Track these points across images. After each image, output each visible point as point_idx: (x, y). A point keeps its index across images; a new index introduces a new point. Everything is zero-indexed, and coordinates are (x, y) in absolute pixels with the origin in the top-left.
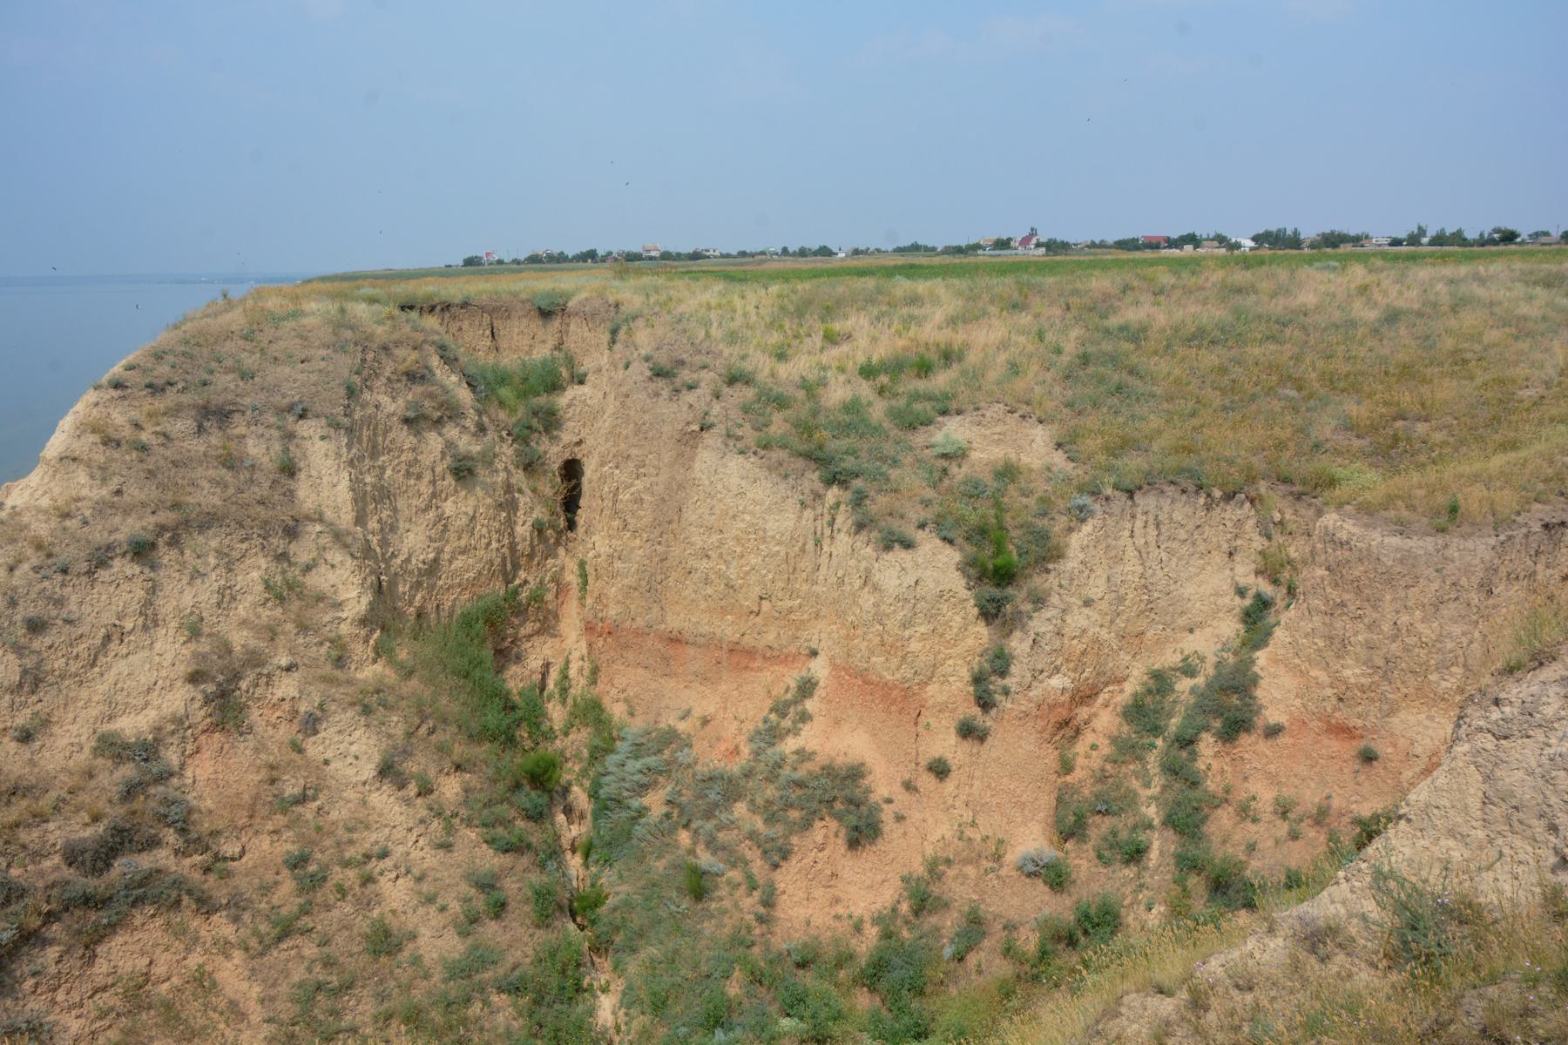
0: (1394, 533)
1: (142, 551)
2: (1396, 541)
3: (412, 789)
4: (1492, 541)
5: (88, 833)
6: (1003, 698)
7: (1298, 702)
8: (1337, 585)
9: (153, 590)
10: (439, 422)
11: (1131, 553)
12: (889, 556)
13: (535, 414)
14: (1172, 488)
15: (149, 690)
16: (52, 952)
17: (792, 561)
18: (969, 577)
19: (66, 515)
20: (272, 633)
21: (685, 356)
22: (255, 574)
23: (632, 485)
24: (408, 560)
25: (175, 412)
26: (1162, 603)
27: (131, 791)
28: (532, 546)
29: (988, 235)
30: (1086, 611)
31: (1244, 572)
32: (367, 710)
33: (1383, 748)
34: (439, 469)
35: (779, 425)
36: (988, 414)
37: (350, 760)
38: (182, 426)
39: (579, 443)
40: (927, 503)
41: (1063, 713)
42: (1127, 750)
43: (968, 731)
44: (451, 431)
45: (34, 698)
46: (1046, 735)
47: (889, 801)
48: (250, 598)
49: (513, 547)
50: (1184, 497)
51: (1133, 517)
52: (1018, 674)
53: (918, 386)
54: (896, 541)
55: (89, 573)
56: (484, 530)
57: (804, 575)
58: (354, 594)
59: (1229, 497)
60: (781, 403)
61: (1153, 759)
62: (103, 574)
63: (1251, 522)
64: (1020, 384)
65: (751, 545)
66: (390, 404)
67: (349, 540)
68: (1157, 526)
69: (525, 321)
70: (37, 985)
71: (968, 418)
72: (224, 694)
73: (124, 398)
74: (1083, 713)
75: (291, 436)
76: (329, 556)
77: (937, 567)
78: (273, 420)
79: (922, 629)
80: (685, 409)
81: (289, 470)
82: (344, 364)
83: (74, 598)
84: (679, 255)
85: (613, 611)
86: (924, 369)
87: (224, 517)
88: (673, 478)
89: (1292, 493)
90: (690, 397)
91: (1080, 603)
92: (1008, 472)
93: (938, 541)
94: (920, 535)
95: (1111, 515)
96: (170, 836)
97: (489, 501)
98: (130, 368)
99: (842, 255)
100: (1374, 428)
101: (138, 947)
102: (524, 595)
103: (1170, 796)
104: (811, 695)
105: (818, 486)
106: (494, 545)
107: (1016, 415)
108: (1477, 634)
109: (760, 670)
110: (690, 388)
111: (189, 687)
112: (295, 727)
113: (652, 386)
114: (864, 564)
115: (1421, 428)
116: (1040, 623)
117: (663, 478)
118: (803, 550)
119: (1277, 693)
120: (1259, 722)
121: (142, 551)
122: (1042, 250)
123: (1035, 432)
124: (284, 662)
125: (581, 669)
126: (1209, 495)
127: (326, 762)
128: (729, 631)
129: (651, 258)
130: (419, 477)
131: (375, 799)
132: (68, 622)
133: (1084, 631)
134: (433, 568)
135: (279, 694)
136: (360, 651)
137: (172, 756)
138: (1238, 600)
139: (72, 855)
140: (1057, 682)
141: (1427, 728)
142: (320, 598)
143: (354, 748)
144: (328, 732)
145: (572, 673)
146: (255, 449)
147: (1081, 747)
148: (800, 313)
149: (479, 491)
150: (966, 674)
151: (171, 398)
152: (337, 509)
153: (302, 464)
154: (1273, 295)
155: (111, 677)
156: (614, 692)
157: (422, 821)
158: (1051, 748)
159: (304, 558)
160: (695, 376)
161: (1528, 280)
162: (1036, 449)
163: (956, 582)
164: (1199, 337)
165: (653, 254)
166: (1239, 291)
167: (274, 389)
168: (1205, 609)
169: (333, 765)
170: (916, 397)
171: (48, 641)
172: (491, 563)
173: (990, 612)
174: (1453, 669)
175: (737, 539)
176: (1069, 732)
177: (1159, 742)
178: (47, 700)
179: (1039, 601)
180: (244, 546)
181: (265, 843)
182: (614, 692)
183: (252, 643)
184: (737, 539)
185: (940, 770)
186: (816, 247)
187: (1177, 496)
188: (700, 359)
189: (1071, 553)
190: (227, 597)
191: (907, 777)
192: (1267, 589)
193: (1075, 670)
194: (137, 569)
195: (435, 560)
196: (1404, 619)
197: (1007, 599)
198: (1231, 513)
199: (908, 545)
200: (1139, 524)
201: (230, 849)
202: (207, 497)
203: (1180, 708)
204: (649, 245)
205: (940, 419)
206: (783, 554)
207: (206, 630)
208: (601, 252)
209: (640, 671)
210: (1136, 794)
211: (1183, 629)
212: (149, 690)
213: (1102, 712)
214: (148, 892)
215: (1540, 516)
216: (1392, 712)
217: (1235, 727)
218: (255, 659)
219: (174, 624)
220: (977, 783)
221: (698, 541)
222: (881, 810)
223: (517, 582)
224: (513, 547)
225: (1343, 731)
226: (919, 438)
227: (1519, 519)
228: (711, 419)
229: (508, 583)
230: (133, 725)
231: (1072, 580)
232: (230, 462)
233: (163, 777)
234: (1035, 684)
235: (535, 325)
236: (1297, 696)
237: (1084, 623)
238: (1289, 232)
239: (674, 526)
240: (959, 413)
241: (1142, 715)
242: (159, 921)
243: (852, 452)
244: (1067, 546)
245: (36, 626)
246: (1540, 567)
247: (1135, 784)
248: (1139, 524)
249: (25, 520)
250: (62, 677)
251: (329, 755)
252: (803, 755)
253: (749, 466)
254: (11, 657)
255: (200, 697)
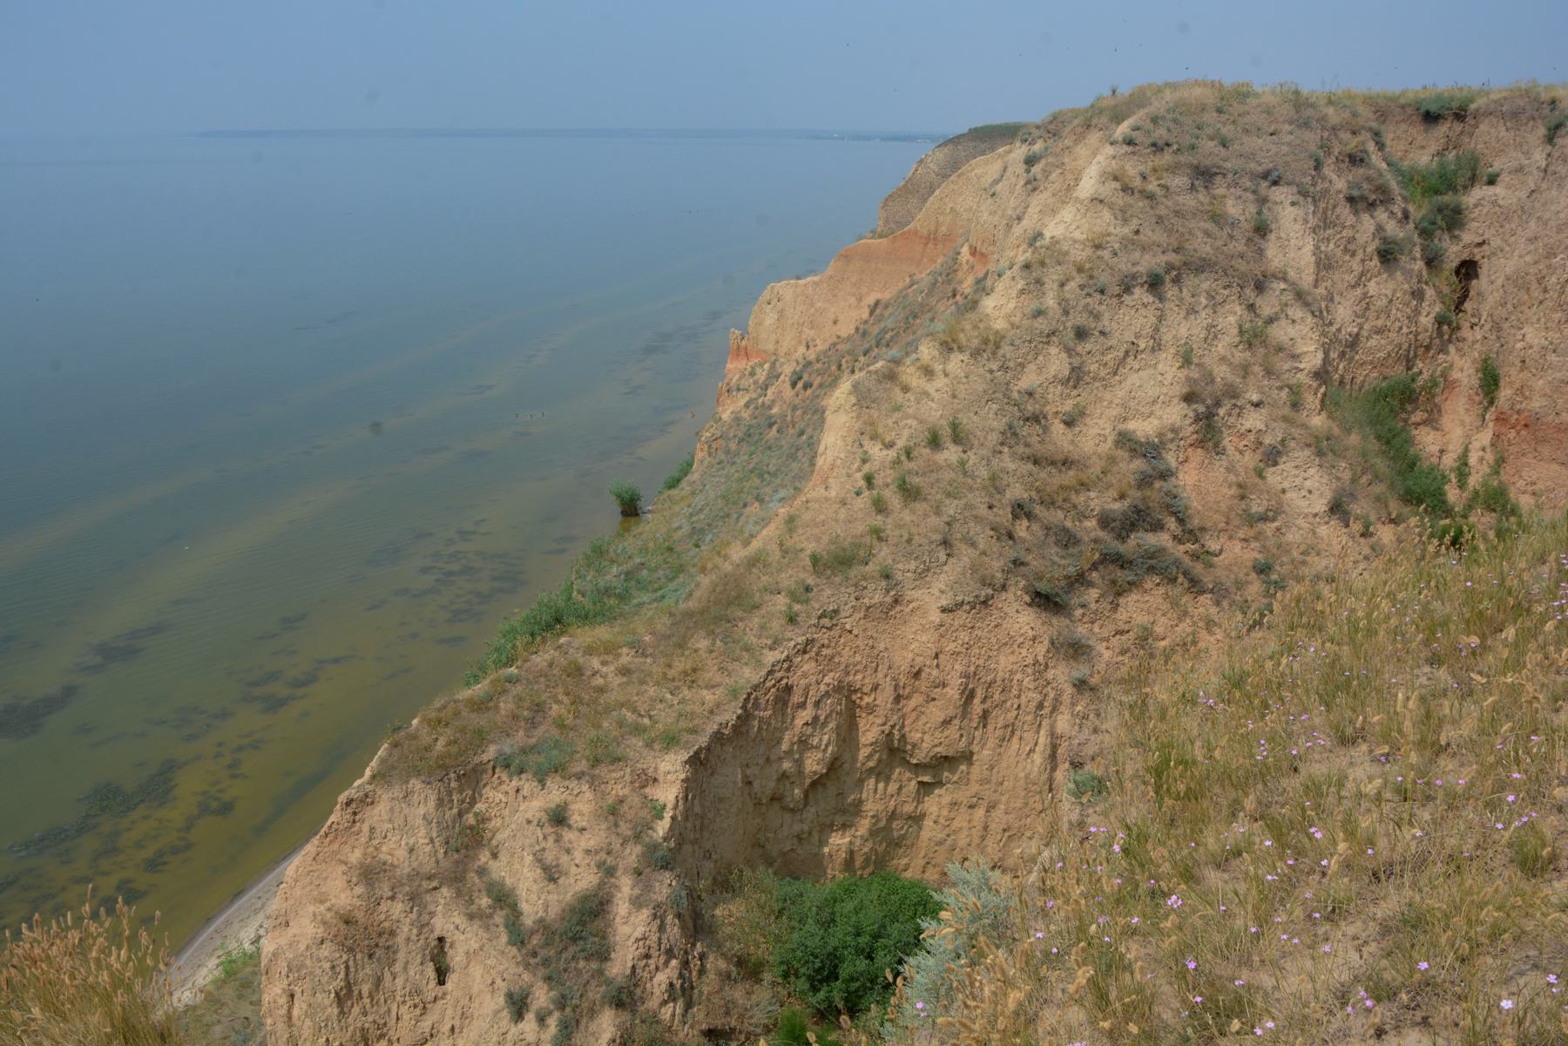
1: (1154, 284)
3: (1356, 527)
5: (1117, 506)
9: (1160, 319)
10: (1372, 206)
13: (1440, 210)
15: (1154, 402)
16: (1094, 593)
19: (1098, 247)
20: (1245, 370)
22: (1232, 319)
24: (1339, 330)
25: (1174, 169)
27: (1144, 481)
28: (1431, 338)
32: (1320, 453)
34: (1369, 250)
37: (1304, 493)
38: (1179, 181)
39: (1480, 245)
44: (1381, 215)
45: (1075, 392)
48: (1227, 339)
55: (1119, 296)
58: (1312, 348)
62: (1127, 299)
66: (1339, 182)
67: (1309, 299)
69: (1403, 126)
70: (1084, 615)
72: (1208, 414)
73: (1133, 153)
75: (1263, 201)
76: (1290, 312)
78: (1248, 184)
81: (1262, 230)
82: (1312, 138)
83: (1107, 315)
85: (1536, 404)
87: (1216, 264)
96: (1171, 523)
97: (1406, 286)
98: (1136, 129)
101: (1146, 607)
102: (1420, 382)
106: (1405, 330)
111: (1184, 405)
112: (1258, 457)
121: (1154, 284)
124: (1255, 398)
125: (1481, 459)
127: (1284, 491)
130: (1353, 255)
131: (1323, 531)
132: (1102, 333)
134: (1354, 342)
135: (1248, 425)
136: (1311, 401)
137: (1171, 459)
139: (1105, 521)
142: (1280, 349)
143: (1308, 483)
144: (1286, 465)
145: (1473, 460)
146: (1232, 208)
151: (1167, 158)
152: (1299, 270)
153: (1273, 226)
155: (1127, 385)
156: (1521, 483)
157: (1366, 558)
159: (1267, 311)
167: (1250, 157)
169: (1288, 495)
171: (1088, 347)
172: (1400, 346)
178: (1085, 395)
180: (1226, 292)
181: (1237, 547)
183: (1230, 377)
190: (1212, 334)
194: (1151, 299)
195: (1358, 335)
201: (1213, 546)
202: (1202, 247)
207: (1196, 360)
212: (1154, 402)
214: (1156, 565)
218: (1232, 393)
219: (1172, 350)
229: (1409, 369)
230: (1143, 428)
232: (1217, 218)
233: (1165, 475)
235: (1416, 131)
242: (1162, 590)
245: (1081, 334)
249: (1065, 248)
250: (1094, 379)
251: (1286, 485)
254: (1064, 355)
255: (1192, 414)
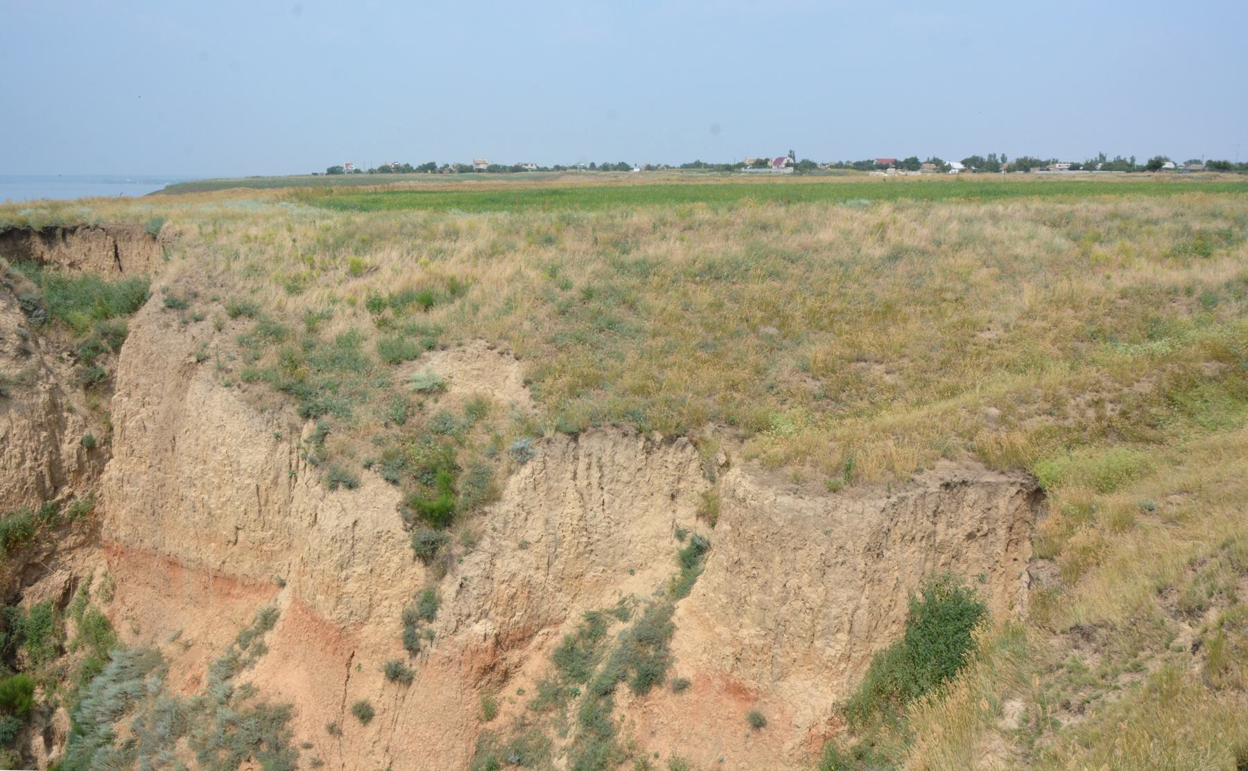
0: (788, 492)
2: (787, 500)
4: (882, 503)
6: (428, 643)
7: (705, 657)
8: (736, 542)
11: (572, 495)
12: (332, 496)
14: (615, 430)
17: (263, 494)
18: (407, 520)
21: (200, 288)
23: (138, 413)
26: (602, 545)
29: (750, 158)
30: (520, 553)
31: (686, 515)
33: (772, 714)
35: (270, 357)
36: (469, 350)
40: (379, 442)
41: (487, 659)
42: (552, 697)
43: (396, 674)
46: (471, 681)
47: (308, 746)
49: (54, 465)
50: (626, 440)
51: (576, 458)
52: (444, 615)
53: (414, 318)
54: (342, 481)
56: (17, 451)
57: (276, 507)
59: (670, 440)
60: (277, 335)
61: (574, 706)
63: (694, 465)
64: (510, 320)
65: (227, 476)
68: (600, 468)
69: (141, 243)
71: (451, 353)
74: (514, 656)
77: (379, 505)
79: (360, 570)
80: (189, 340)
84: (505, 167)
86: (428, 304)
88: (170, 407)
89: (736, 436)
90: (194, 329)
91: (514, 545)
92: (478, 409)
93: (382, 481)
94: (366, 475)
95: (552, 457)
97: (24, 422)
99: (636, 170)
100: (828, 370)
102: (65, 512)
103: (585, 747)
104: (271, 627)
105: (297, 419)
106: (28, 464)
107: (495, 351)
108: (864, 601)
109: (239, 597)
110: (197, 320)
113: (164, 318)
114: (313, 502)
115: (878, 369)
116: (470, 567)
117: (163, 407)
118: (275, 482)
119: (689, 651)
120: (669, 676)
122: (791, 170)
123: (511, 368)
126: (648, 439)
128: (211, 559)
129: (480, 171)
133: (514, 575)
138: (676, 542)
140: (480, 628)
141: (811, 695)
147: (509, 691)
148: (339, 244)
149: (13, 413)
150: (397, 613)
154: (796, 231)
158: (475, 693)
160: (204, 308)
161: (1039, 219)
162: (506, 386)
163: (395, 523)
164: (711, 273)
165: (482, 167)
166: (764, 228)
168: (646, 550)
170: (413, 331)
173: (427, 553)
174: (839, 636)
175: (215, 471)
176: (496, 677)
177: (583, 689)
179: (471, 544)
182: (124, 609)
184: (215, 471)
185: (364, 714)
186: (616, 163)
187: (619, 438)
188: (214, 291)
189: (507, 495)
191: (332, 719)
192: (702, 529)
193: (504, 614)
196: (793, 582)
197: (443, 541)
198: (673, 456)
199: (351, 486)
200: (582, 466)
203: (607, 654)
204: (479, 159)
205: (426, 354)
206: (253, 487)
208: (439, 165)
209: (149, 590)
210: (550, 744)
211: (624, 570)
213: (533, 655)
215: (940, 474)
216: (783, 676)
217: (647, 681)
220: (398, 728)
221: (186, 469)
222: (298, 756)
223: (59, 497)
224: (54, 465)
225: (738, 690)
226: (401, 373)
227: (917, 477)
228: (208, 352)
231: (506, 523)
234: (461, 628)
236: (705, 651)
237: (514, 567)
238: (986, 158)
239: (169, 454)
240: (444, 348)
241: (571, 659)
243: (334, 388)
244: (505, 486)
246: (941, 527)
247: (552, 733)
248: (582, 466)
252: (249, 690)
253: (231, 398)
